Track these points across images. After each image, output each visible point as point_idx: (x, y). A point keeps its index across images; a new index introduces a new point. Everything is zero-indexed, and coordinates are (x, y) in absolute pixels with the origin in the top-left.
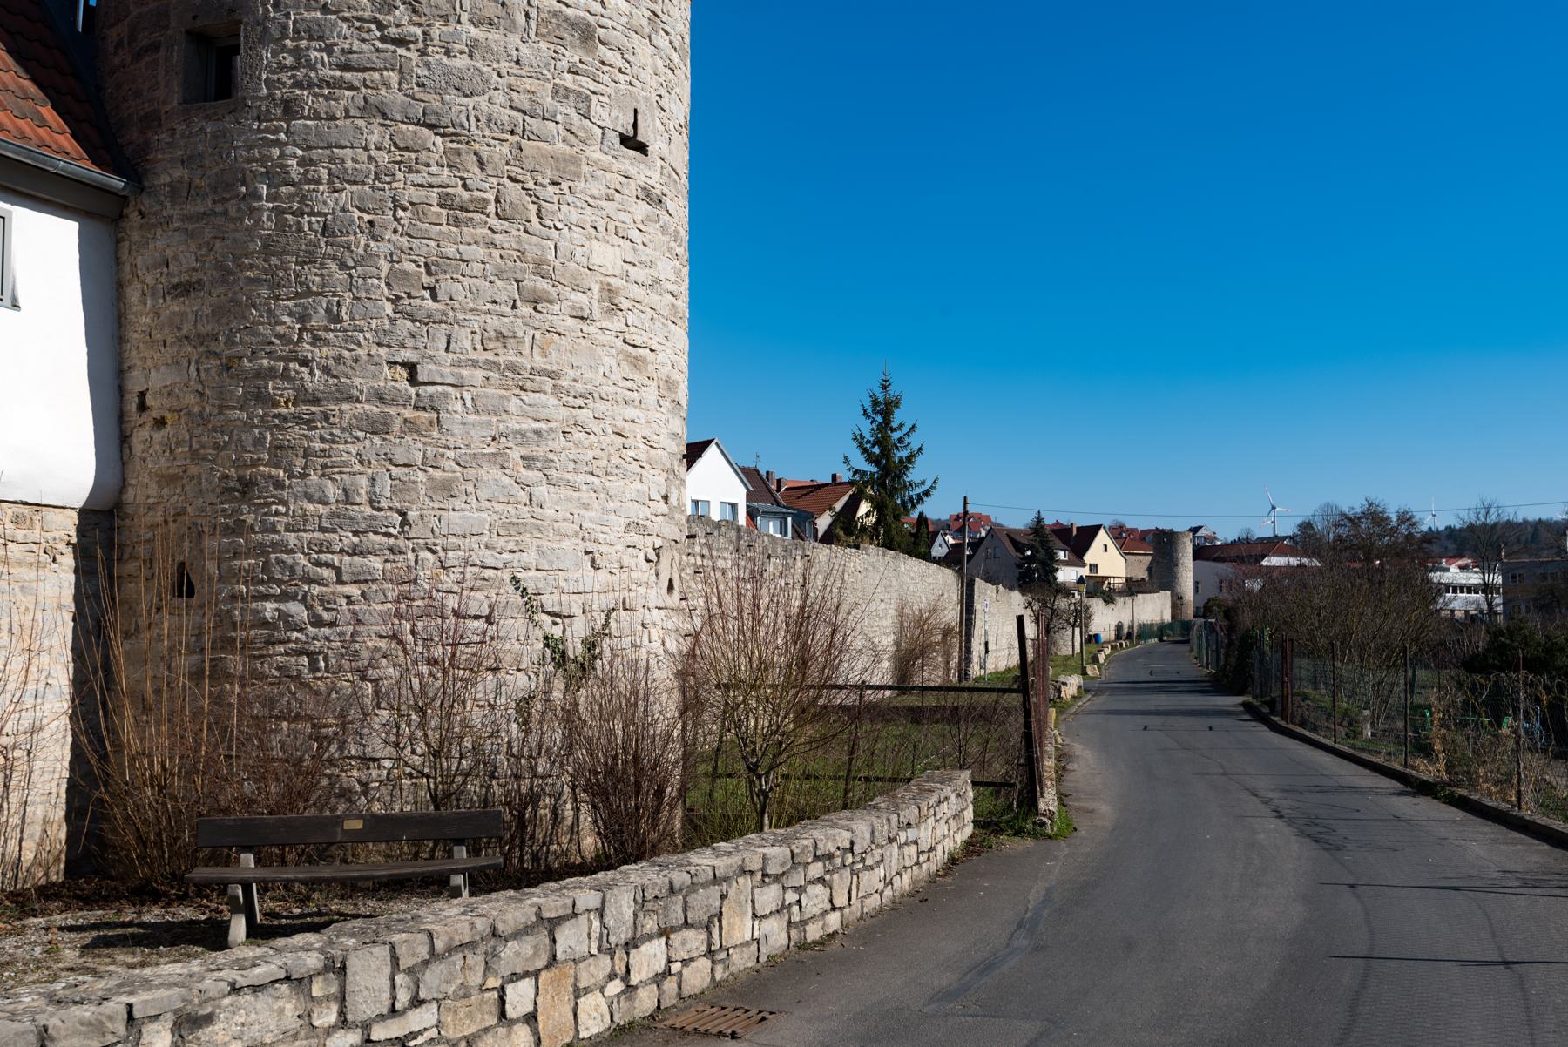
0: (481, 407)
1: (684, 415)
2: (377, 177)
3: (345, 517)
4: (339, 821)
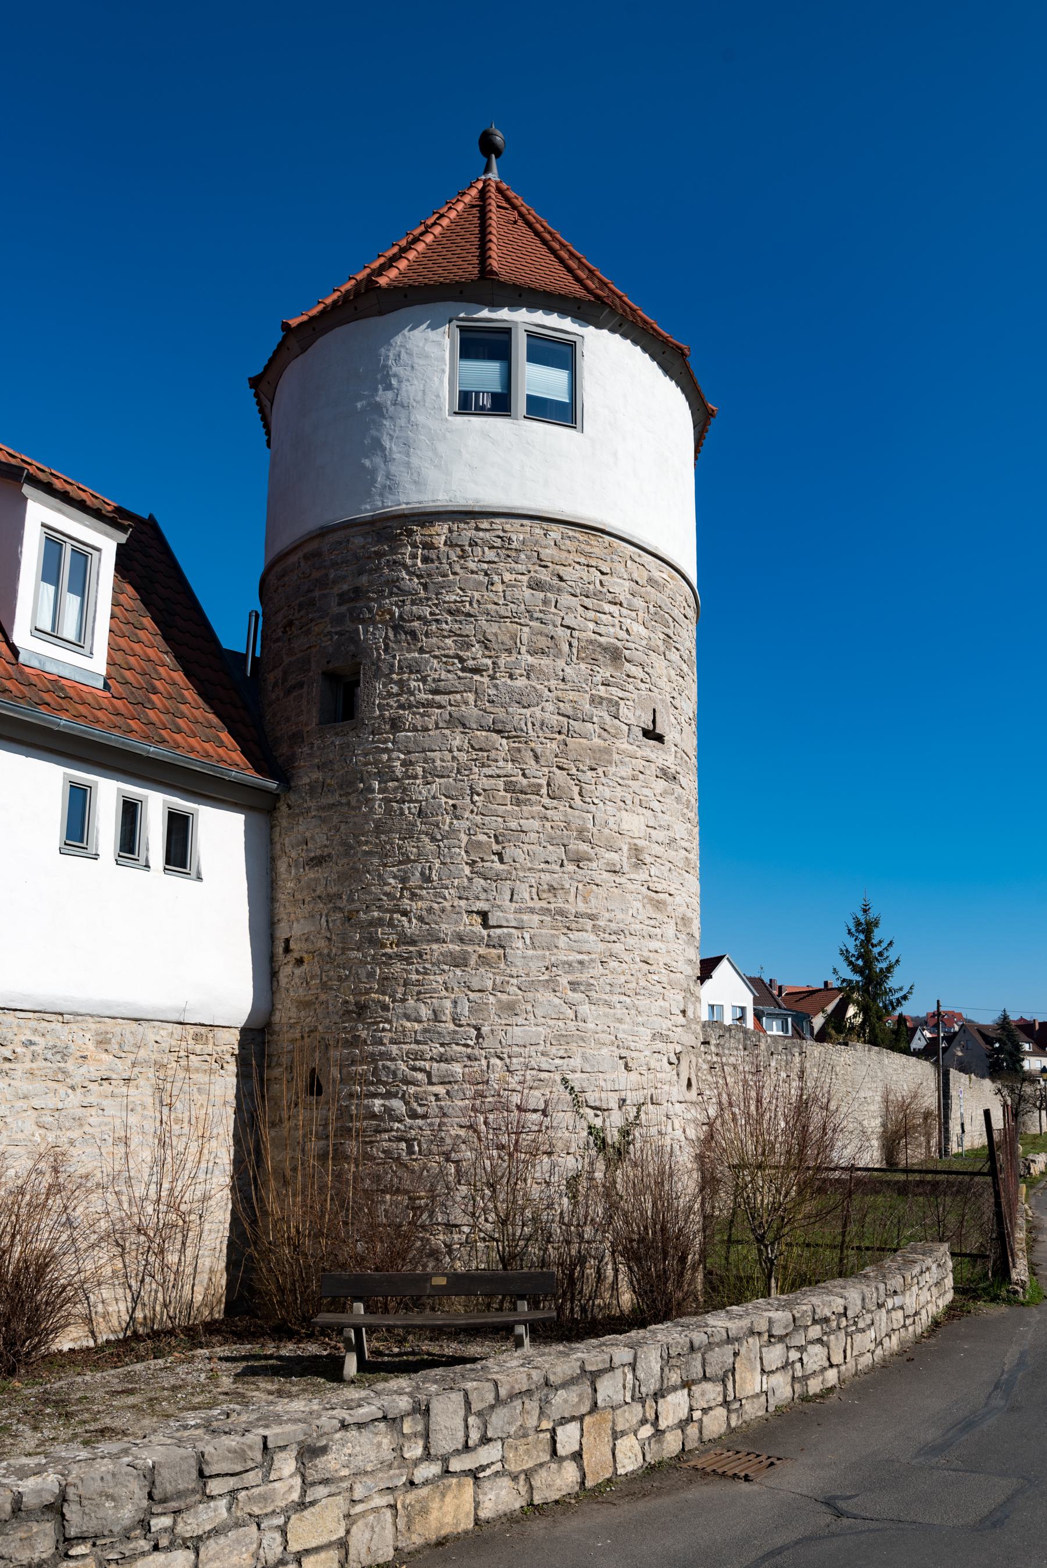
0: (537, 944)
1: (697, 945)
2: (459, 772)
3: (434, 1032)
4: (428, 1277)
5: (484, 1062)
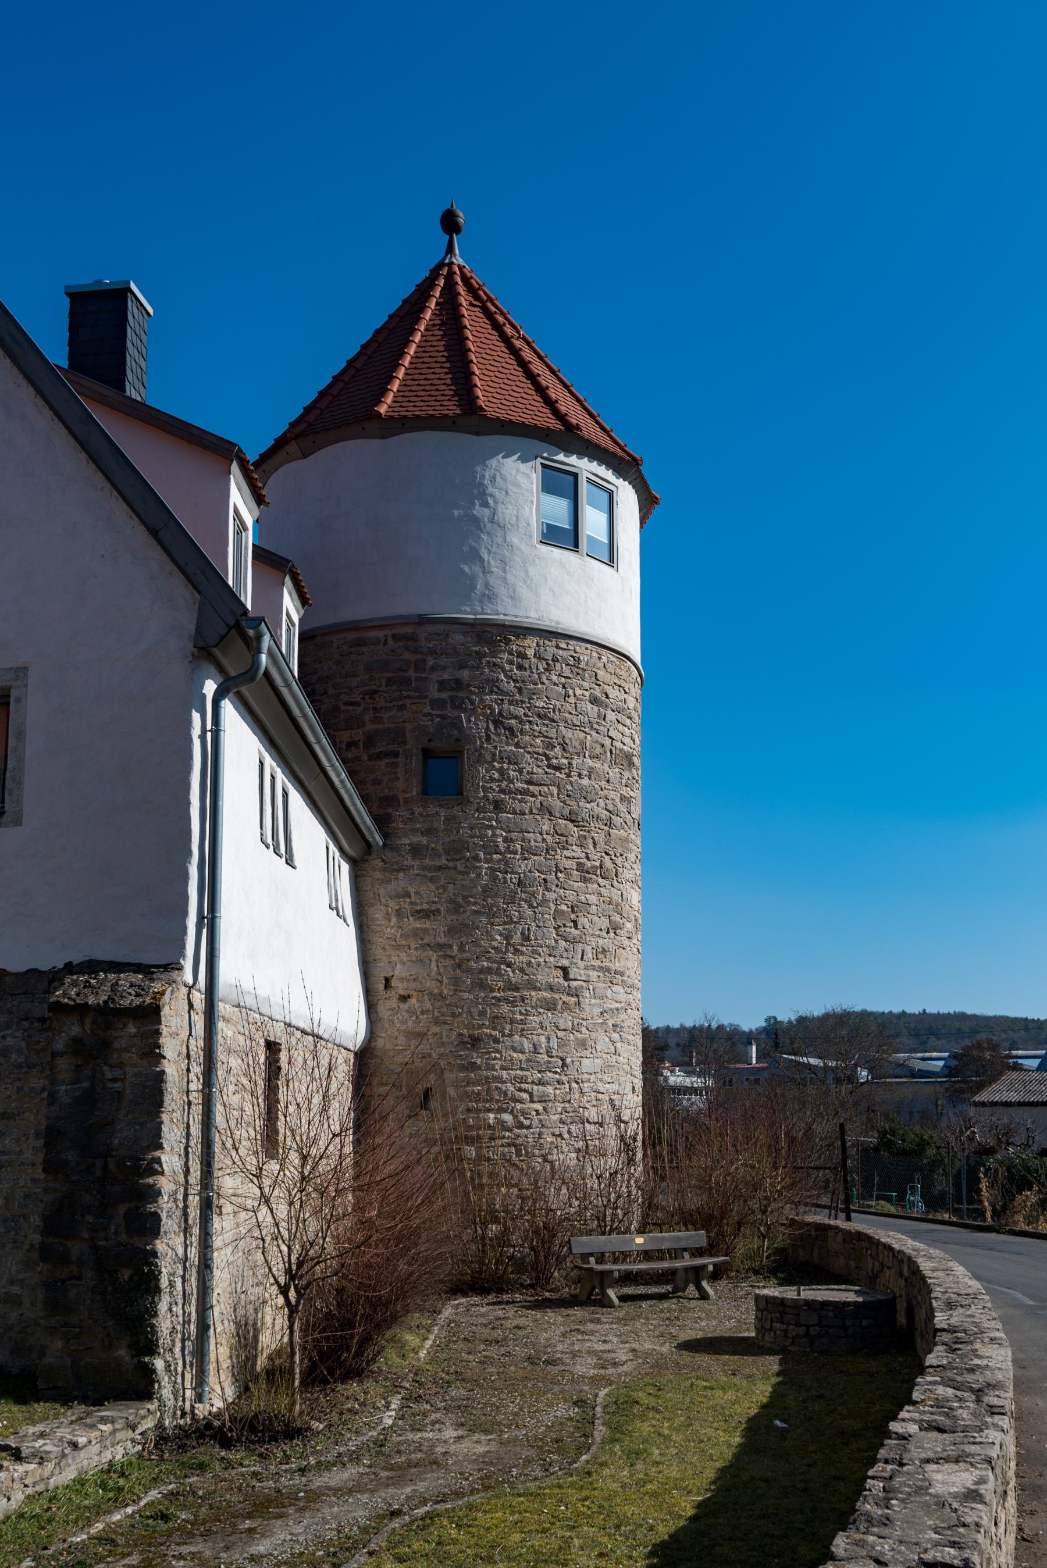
2: (548, 852)
5: (567, 1086)
